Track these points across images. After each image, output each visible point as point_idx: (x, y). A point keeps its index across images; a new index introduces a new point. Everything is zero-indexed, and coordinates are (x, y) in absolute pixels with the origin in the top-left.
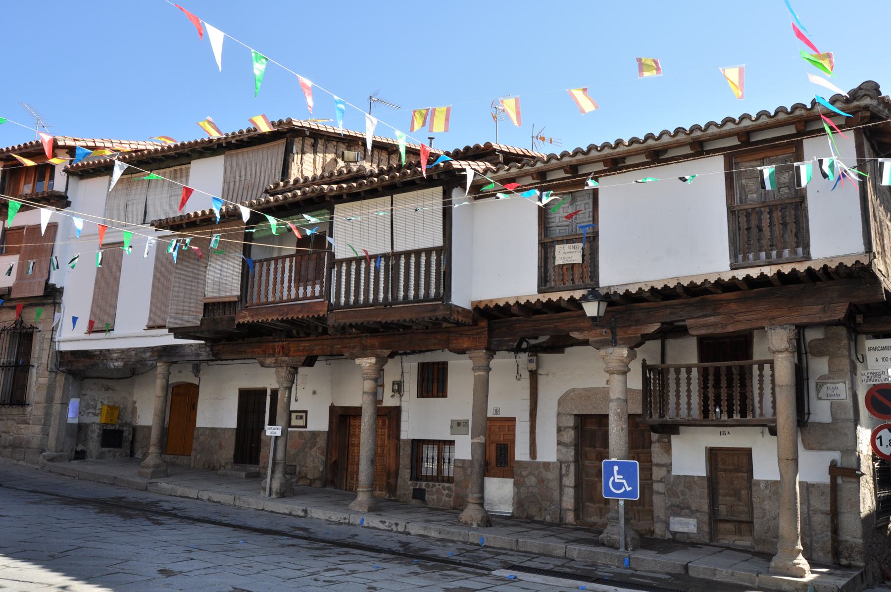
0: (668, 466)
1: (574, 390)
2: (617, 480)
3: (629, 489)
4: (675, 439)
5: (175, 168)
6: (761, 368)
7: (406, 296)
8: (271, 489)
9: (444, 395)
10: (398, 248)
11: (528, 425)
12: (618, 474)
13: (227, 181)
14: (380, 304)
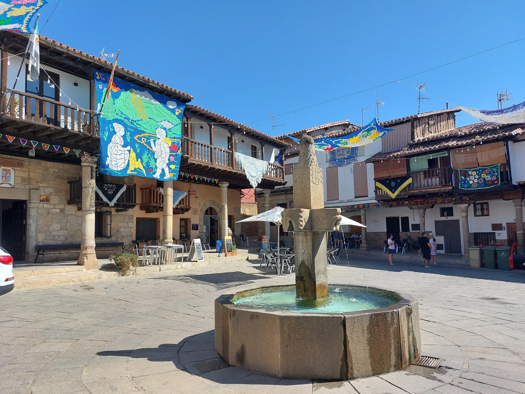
7: (379, 194)
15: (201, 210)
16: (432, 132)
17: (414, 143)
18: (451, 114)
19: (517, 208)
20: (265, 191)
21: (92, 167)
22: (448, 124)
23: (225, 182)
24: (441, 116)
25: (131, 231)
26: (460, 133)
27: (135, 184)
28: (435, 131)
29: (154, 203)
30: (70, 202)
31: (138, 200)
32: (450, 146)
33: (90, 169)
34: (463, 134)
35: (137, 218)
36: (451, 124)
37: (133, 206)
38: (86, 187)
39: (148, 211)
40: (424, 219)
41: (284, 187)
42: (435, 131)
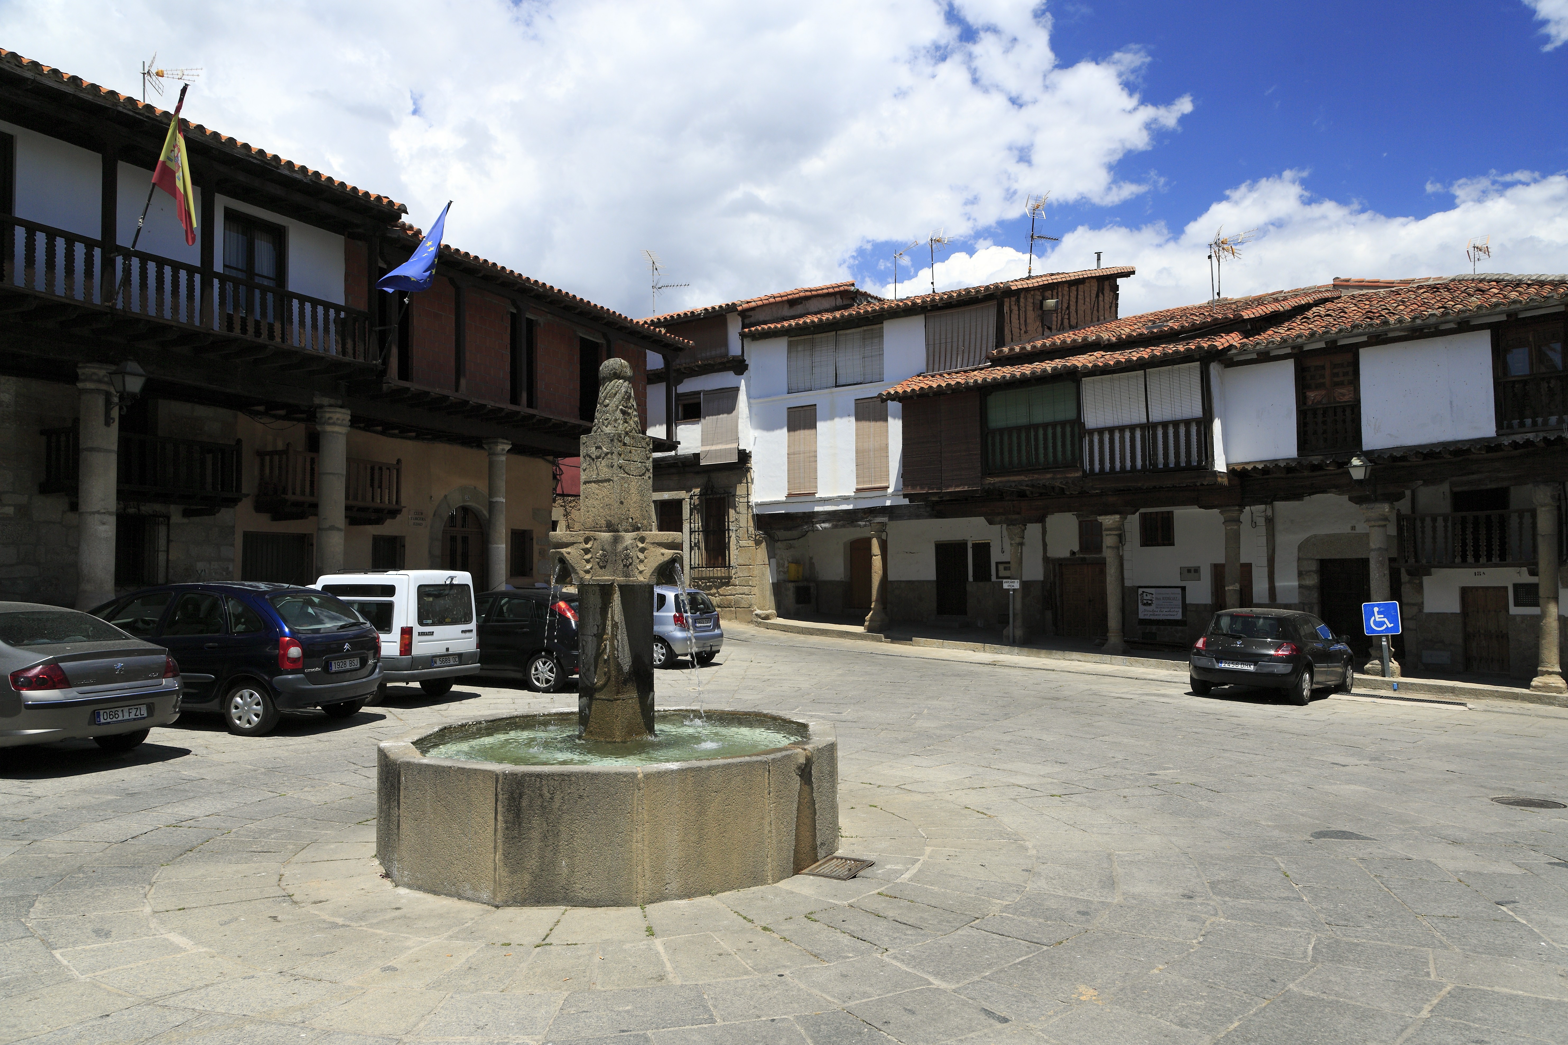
0: (1421, 605)
1: (1315, 536)
2: (1377, 620)
3: (1390, 626)
4: (1426, 580)
5: (865, 328)
6: (1521, 517)
7: (1166, 464)
8: (1014, 636)
9: (1173, 544)
10: (1155, 417)
11: (1265, 571)
12: (424, 591)
13: (931, 342)
14: (1139, 471)
15: (434, 515)
16: (1054, 327)
17: (1001, 355)
18: (1107, 283)
19: (1228, 528)
21: (108, 395)
22: (1098, 307)
23: (500, 440)
24: (1081, 287)
25: (228, 568)
27: (239, 441)
28: (1062, 323)
29: (294, 493)
30: (45, 489)
31: (249, 483)
33: (101, 401)
34: (1114, 339)
35: (246, 535)
36: (1107, 306)
37: (232, 502)
38: (91, 449)
39: (278, 515)
42: (1062, 323)
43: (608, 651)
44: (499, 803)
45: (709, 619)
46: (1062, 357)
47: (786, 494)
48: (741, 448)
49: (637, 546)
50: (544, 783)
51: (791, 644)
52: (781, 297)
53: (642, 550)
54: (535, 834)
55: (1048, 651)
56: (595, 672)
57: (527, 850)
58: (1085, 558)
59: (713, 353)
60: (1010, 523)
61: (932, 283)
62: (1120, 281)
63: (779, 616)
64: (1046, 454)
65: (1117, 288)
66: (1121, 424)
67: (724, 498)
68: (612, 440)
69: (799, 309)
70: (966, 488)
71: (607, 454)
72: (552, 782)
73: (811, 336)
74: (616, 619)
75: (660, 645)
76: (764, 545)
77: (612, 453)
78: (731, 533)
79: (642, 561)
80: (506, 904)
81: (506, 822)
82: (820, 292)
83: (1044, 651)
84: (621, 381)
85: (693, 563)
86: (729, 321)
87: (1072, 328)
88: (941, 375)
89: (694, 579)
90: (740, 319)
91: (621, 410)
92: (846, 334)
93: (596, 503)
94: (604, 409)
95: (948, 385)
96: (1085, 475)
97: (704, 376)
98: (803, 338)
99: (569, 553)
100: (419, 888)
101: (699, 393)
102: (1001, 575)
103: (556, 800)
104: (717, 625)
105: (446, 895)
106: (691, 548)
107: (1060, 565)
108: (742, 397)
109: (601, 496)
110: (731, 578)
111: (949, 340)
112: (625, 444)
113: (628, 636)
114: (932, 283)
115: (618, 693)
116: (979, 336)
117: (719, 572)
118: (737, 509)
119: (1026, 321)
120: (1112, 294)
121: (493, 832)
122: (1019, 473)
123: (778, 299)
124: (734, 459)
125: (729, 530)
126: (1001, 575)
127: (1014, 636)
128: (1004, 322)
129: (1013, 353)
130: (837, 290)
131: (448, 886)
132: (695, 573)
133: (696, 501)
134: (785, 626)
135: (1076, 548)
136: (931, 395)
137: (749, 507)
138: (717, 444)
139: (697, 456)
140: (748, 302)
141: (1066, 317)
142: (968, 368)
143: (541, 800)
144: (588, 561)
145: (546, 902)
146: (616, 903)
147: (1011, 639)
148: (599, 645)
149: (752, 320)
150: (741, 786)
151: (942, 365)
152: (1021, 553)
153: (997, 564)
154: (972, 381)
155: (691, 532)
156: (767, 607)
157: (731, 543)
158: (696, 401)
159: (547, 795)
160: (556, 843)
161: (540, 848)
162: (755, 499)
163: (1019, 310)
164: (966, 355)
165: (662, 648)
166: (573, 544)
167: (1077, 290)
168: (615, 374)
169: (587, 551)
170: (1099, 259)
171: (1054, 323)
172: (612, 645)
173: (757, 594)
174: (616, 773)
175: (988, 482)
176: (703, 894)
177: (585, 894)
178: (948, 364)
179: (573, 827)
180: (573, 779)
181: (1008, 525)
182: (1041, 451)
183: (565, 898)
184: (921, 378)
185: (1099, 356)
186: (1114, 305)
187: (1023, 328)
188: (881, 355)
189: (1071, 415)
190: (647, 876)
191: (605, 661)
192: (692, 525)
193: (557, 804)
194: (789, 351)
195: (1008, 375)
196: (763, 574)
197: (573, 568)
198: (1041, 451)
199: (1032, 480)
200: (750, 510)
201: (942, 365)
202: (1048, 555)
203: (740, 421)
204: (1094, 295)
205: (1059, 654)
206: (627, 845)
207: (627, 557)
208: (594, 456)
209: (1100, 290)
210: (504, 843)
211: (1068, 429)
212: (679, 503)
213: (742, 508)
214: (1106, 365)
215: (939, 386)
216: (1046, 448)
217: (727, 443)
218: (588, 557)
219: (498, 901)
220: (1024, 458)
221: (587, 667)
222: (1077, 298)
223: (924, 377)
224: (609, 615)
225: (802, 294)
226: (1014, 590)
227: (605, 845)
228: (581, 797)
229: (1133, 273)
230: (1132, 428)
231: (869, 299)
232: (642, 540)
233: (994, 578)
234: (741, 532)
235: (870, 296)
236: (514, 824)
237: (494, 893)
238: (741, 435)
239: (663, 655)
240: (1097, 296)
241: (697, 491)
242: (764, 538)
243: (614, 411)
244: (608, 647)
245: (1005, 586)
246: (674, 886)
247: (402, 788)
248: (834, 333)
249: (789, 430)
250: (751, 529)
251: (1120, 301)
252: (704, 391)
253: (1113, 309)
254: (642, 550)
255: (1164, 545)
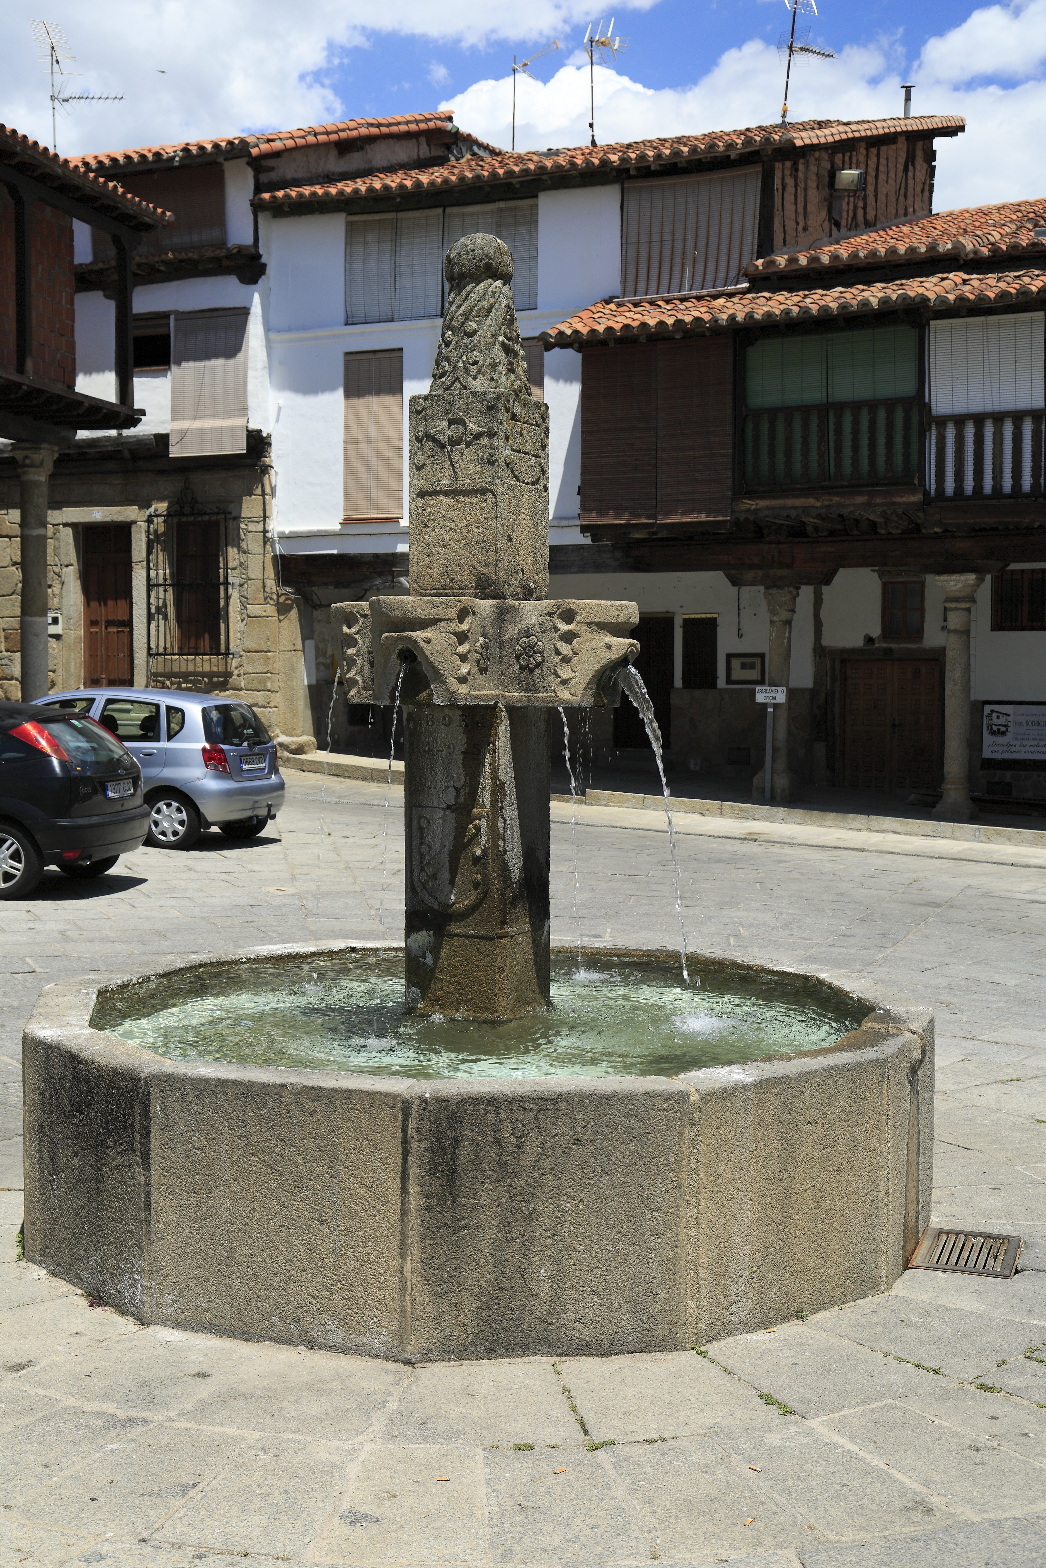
5: (502, 205)
8: (773, 789)
13: (633, 239)
14: (1027, 496)
17: (771, 270)
20: (26, 453)
22: (906, 189)
24: (884, 149)
26: (971, 246)
32: (929, 300)
36: (918, 189)
40: (787, 635)
41: (120, 435)
42: (855, 217)
43: (484, 839)
44: (411, 1159)
45: (262, 755)
46: (887, 279)
47: (341, 517)
48: (253, 426)
49: (556, 629)
50: (503, 1115)
51: (362, 800)
52: (328, 133)
53: (568, 638)
54: (486, 1218)
55: (841, 815)
56: (452, 883)
57: (469, 1250)
58: (891, 649)
59: (196, 238)
60: (771, 584)
61: (591, 125)
62: (939, 143)
63: (322, 746)
64: (855, 460)
65: (932, 155)
66: (997, 408)
67: (217, 524)
68: (492, 408)
69: (355, 161)
70: (703, 517)
71: (480, 435)
72: (519, 1115)
73: (392, 215)
74: (502, 775)
75: (175, 804)
76: (294, 613)
77: (491, 435)
78: (230, 591)
79: (566, 660)
80: (428, 1357)
81: (426, 1196)
82: (394, 129)
83: (833, 815)
84: (499, 283)
85: (153, 645)
86: (228, 175)
87: (870, 225)
88: (652, 303)
89: (156, 675)
90: (250, 173)
91: (503, 344)
92: (464, 215)
93: (448, 537)
94: (466, 340)
95: (679, 322)
96: (928, 500)
97: (175, 284)
98: (377, 217)
99: (428, 641)
100: (205, 1328)
101: (166, 316)
102: (735, 676)
103: (527, 1149)
104: (274, 769)
105: (275, 1340)
106: (150, 617)
107: (843, 661)
108: (255, 328)
109: (462, 524)
110: (230, 674)
111: (667, 237)
112: (514, 417)
113: (519, 809)
114: (591, 125)
115: (504, 923)
116: (725, 231)
117: (206, 663)
118: (243, 545)
119: (805, 207)
120: (925, 166)
121: (396, 1217)
122: (804, 492)
123: (322, 138)
124: (239, 447)
125: (226, 583)
126: (735, 676)
127: (773, 789)
128: (773, 207)
129: (794, 267)
130: (423, 126)
131: (280, 1324)
132: (158, 665)
133: (159, 524)
134: (338, 766)
135: (876, 631)
136: (643, 339)
137: (266, 540)
138: (205, 417)
139: (162, 440)
140: (269, 141)
141: (861, 204)
142: (704, 292)
143: (497, 1150)
144: (463, 658)
145: (507, 1349)
146: (646, 1346)
147: (768, 794)
148: (461, 829)
149: (273, 176)
150: (848, 1109)
151: (653, 284)
152: (790, 638)
153: (729, 657)
154: (725, 317)
155: (150, 587)
156: (299, 731)
157: (231, 609)
158: (160, 331)
159: (510, 1140)
160: (528, 1234)
161: (495, 1245)
162: (278, 525)
163: (796, 186)
164: (700, 267)
165: (179, 810)
166: (435, 622)
167: (878, 156)
168: (488, 266)
169: (462, 637)
170: (908, 99)
171: (844, 215)
172: (493, 829)
173: (282, 705)
174: (648, 1094)
175: (743, 507)
176: (786, 1320)
177: (585, 1332)
178: (665, 282)
179: (562, 1201)
180: (563, 1106)
181: (767, 588)
182: (847, 452)
183: (544, 1341)
184: (612, 306)
185: (959, 281)
186: (927, 188)
187: (801, 219)
188: (534, 258)
189: (906, 387)
190: (703, 1292)
191: (476, 860)
192: (153, 573)
193: (529, 1156)
194: (349, 243)
195: (796, 309)
196: (293, 670)
197: (436, 671)
198: (847, 452)
199: (829, 506)
200: (268, 547)
201: (653, 284)
202: (826, 642)
203: (251, 374)
204: (901, 167)
205: (861, 820)
206: (669, 1234)
207: (530, 651)
208: (444, 440)
209: (910, 159)
210: (423, 1237)
211: (899, 415)
212: (124, 529)
213: (252, 542)
214: (982, 298)
215: (661, 323)
216: (856, 448)
217: (224, 415)
218: (463, 649)
219: (411, 1350)
220: (814, 465)
221: (430, 871)
222: (877, 169)
223: (619, 305)
224: (487, 768)
225: (364, 131)
226: (776, 706)
227: (626, 1235)
228: (577, 1142)
229: (962, 129)
230: (1018, 417)
231: (475, 148)
232: (569, 616)
233: (721, 683)
234: (251, 589)
235: (476, 142)
236: (443, 1198)
237: (402, 1337)
238: (252, 402)
239: (182, 823)
240: (906, 170)
241: (162, 507)
242: (295, 601)
243: (490, 346)
244: (484, 831)
245: (760, 698)
246: (743, 1308)
247: (154, 1127)
248: (440, 211)
249: (348, 395)
250: (271, 584)
251: (937, 181)
252: (177, 313)
253: (927, 193)
254: (568, 638)
255: (1033, 629)
